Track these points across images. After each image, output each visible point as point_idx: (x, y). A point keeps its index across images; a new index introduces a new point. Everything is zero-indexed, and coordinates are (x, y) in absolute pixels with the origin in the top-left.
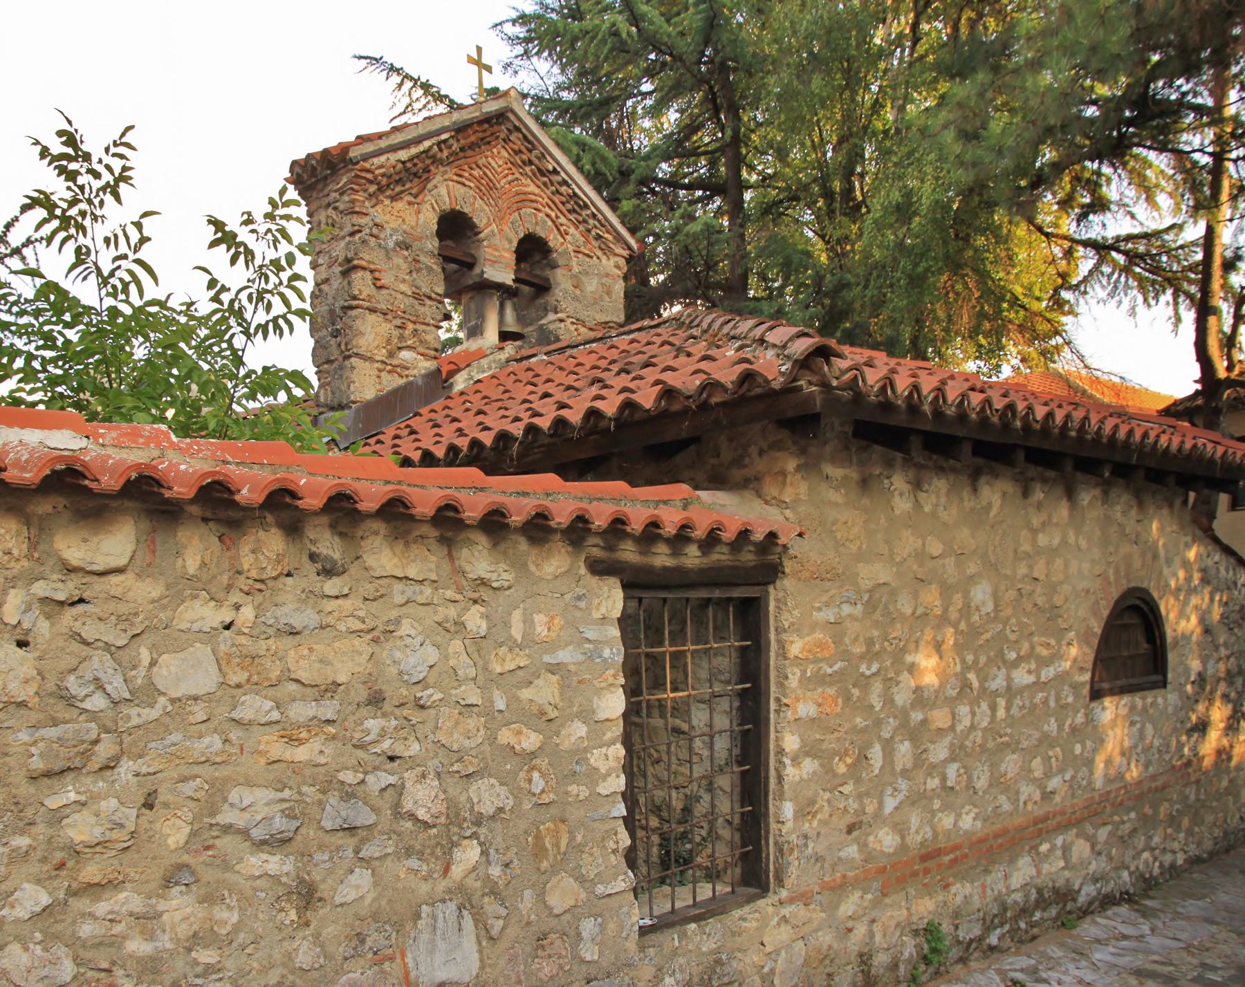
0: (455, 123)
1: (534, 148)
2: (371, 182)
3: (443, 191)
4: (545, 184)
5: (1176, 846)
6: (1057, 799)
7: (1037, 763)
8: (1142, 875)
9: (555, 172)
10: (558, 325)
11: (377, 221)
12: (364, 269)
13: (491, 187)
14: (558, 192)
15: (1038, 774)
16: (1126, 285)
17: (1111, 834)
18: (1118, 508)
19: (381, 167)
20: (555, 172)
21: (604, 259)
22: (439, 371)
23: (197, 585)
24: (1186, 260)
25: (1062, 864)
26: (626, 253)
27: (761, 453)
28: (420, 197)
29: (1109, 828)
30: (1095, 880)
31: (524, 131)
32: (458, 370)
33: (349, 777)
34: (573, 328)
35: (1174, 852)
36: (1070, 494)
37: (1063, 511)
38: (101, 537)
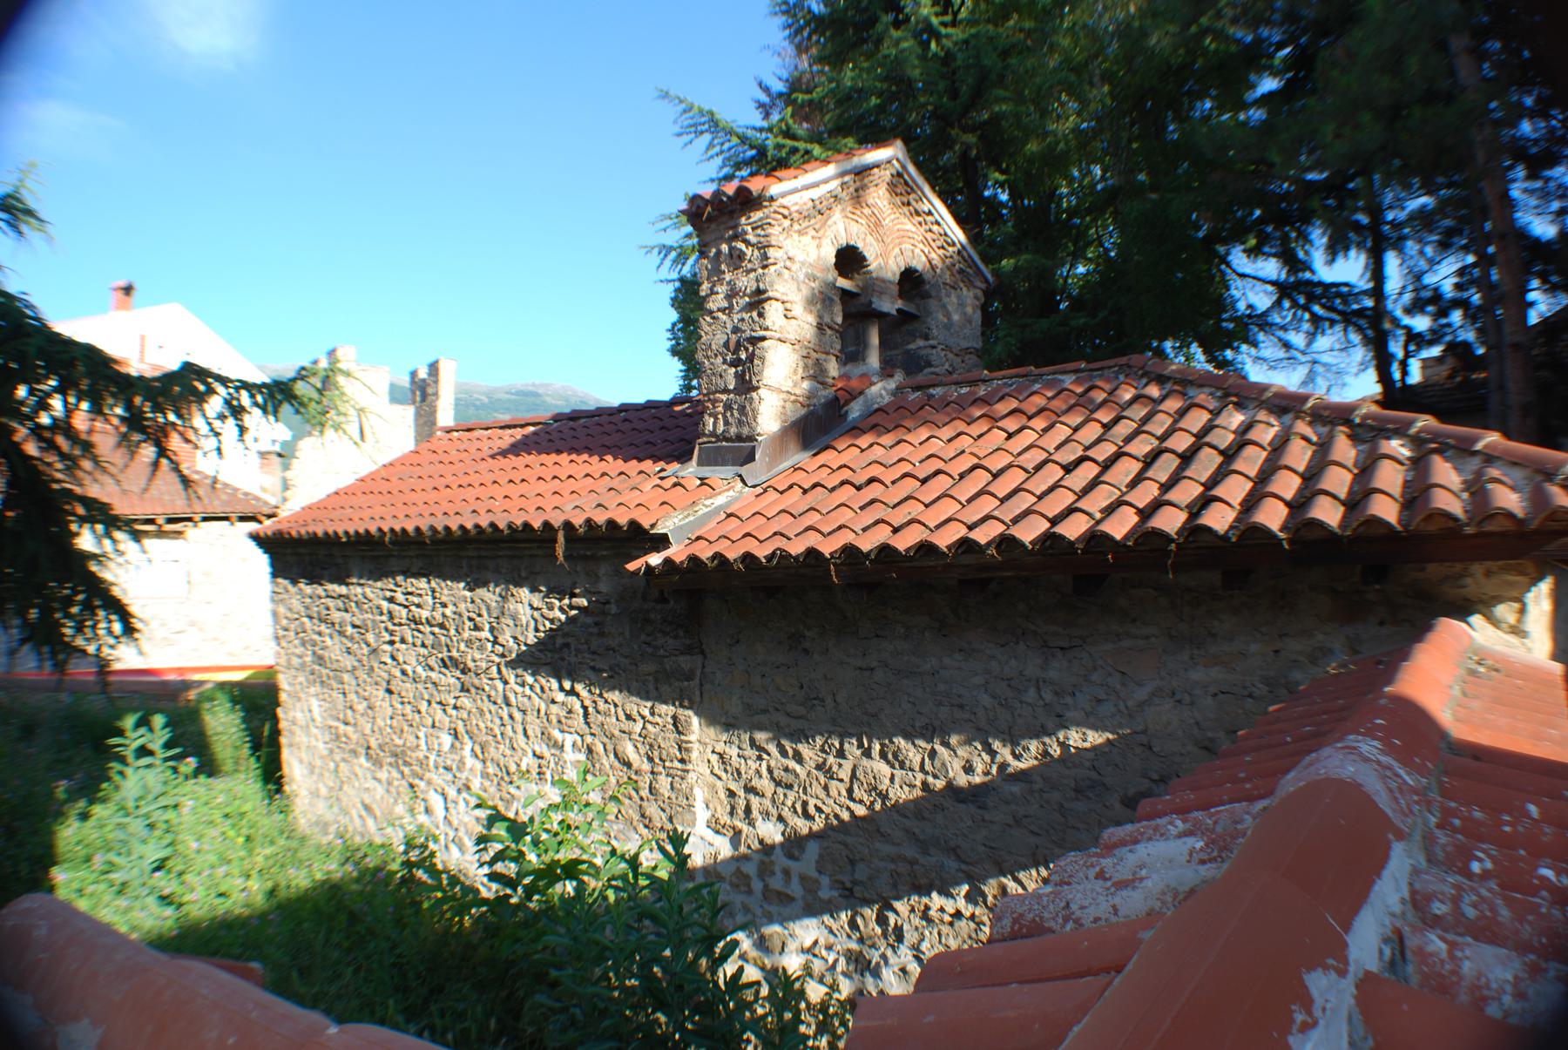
0: (855, 167)
2: (785, 217)
3: (841, 227)
4: (920, 224)
9: (930, 213)
10: (929, 351)
11: (790, 254)
12: (777, 300)
14: (930, 231)
19: (796, 204)
20: (930, 213)
21: (965, 289)
22: (836, 399)
24: (1274, 11)
26: (983, 286)
27: (1488, 574)
28: (821, 232)
31: (906, 177)
32: (854, 398)
34: (943, 354)
38: (210, 733)
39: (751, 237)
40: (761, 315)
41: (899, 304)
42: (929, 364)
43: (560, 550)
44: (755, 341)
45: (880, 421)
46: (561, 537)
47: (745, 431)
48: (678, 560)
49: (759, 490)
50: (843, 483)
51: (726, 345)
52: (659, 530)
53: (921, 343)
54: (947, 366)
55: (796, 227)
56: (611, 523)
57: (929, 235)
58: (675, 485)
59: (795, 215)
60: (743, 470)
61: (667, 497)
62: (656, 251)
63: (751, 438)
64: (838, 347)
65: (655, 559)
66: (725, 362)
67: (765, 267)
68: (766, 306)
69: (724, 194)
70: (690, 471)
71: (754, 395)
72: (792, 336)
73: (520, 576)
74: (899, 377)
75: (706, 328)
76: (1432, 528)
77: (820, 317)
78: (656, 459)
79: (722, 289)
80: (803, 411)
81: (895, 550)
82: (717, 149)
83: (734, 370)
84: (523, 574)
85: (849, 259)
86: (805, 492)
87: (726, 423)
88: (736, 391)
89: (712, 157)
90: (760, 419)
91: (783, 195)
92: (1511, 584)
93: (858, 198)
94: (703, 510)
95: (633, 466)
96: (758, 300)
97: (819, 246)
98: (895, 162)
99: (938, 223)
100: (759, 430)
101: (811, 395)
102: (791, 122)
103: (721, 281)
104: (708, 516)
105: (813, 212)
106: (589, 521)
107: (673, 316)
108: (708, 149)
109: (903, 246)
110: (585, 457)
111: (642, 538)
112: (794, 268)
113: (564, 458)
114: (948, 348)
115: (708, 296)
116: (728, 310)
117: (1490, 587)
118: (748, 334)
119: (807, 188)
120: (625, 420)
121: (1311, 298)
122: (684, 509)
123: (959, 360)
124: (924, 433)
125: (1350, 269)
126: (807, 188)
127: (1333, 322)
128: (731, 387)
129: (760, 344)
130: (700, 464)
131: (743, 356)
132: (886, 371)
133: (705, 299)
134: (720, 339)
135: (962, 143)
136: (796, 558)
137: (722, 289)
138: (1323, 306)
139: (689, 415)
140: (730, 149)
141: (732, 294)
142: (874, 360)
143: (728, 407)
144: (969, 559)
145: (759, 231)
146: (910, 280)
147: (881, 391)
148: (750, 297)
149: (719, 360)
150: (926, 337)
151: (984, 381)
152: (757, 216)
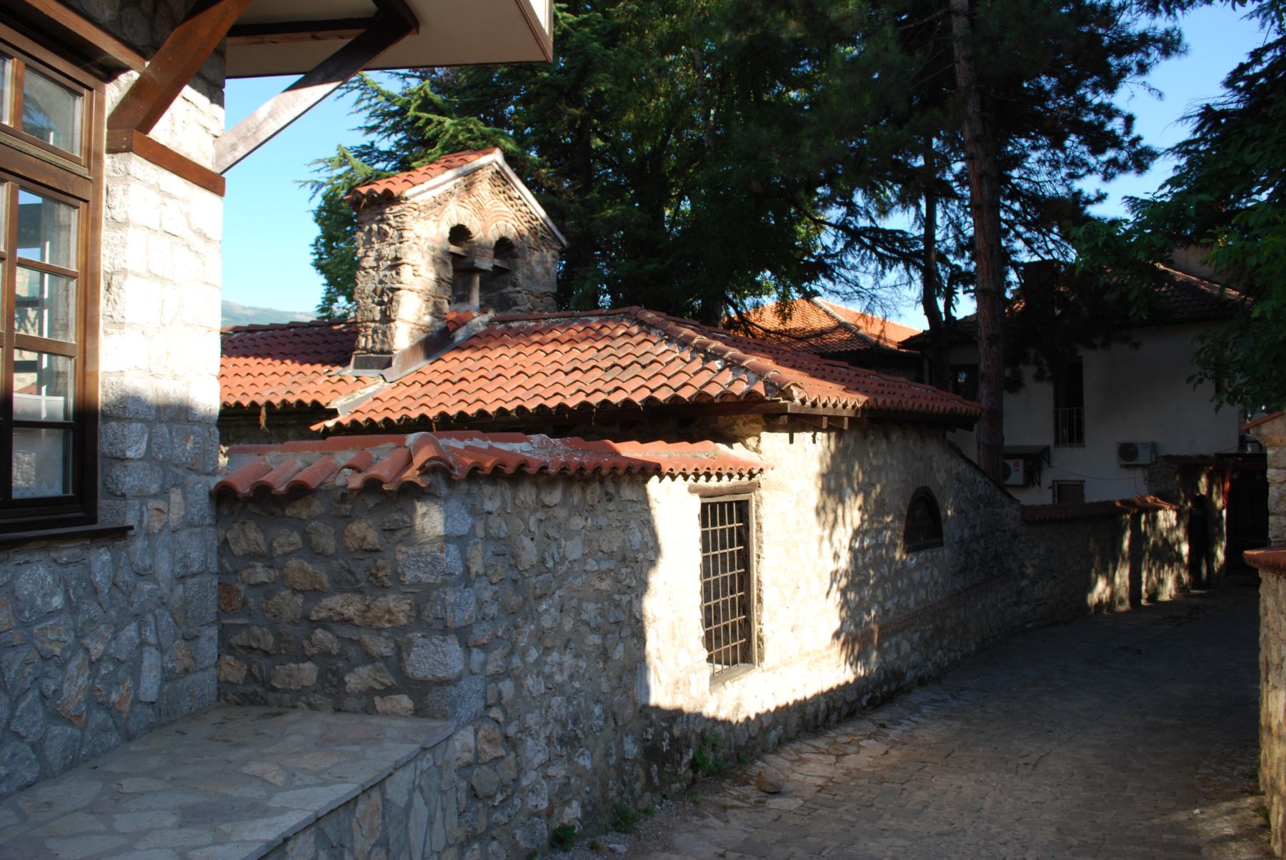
1: (507, 183)
5: (956, 648)
6: (891, 614)
7: (879, 592)
8: (939, 665)
9: (520, 198)
10: (516, 295)
13: (481, 208)
15: (880, 599)
16: (870, 258)
17: (921, 637)
18: (911, 442)
21: (545, 250)
22: (447, 328)
23: (576, 511)
25: (896, 656)
26: (559, 248)
27: (744, 424)
29: (919, 634)
30: (914, 668)
32: (459, 327)
33: (616, 597)
34: (526, 297)
35: (955, 651)
36: (887, 436)
37: (884, 446)
39: (392, 222)
40: (398, 274)
41: (497, 262)
42: (516, 304)
43: (263, 420)
44: (393, 290)
45: (476, 342)
46: (263, 412)
47: (386, 347)
48: (344, 423)
49: (395, 385)
50: (445, 381)
51: (375, 291)
52: (332, 406)
53: (510, 289)
54: (529, 305)
55: (423, 215)
56: (300, 403)
57: (519, 214)
58: (340, 380)
59: (422, 208)
60: (384, 372)
61: (335, 387)
62: (309, 185)
63: (390, 352)
64: (449, 294)
65: (330, 424)
66: (373, 302)
67: (401, 243)
68: (401, 268)
69: (375, 192)
70: (349, 372)
71: (392, 324)
72: (418, 288)
73: (228, 439)
74: (491, 314)
75: (362, 279)
76: (704, 401)
77: (438, 274)
78: (324, 364)
79: (372, 254)
80: (424, 336)
81: (466, 414)
82: (365, 103)
83: (379, 308)
84: (231, 438)
85: (459, 233)
86: (423, 385)
87: (374, 342)
88: (381, 321)
89: (360, 110)
90: (396, 340)
91: (414, 196)
92: (754, 429)
93: (469, 187)
94: (358, 396)
95: (307, 368)
96: (396, 264)
97: (438, 226)
98: (494, 164)
99: (525, 205)
100: (395, 347)
101: (432, 325)
102: (428, 90)
103: (372, 248)
104: (362, 399)
105: (434, 204)
106: (284, 401)
107: (316, 231)
108: (357, 103)
109: (499, 223)
110: (269, 360)
111: (320, 411)
112: (421, 242)
113: (251, 360)
114: (530, 293)
115: (362, 257)
116: (377, 268)
117: (745, 430)
118: (389, 285)
119: (429, 189)
120: (295, 335)
121: (875, 241)
122: (347, 395)
123: (539, 301)
124: (500, 351)
125: (902, 221)
126: (429, 189)
127: (896, 261)
128: (377, 319)
129: (397, 293)
130: (356, 367)
131: (386, 299)
132: (483, 309)
133: (361, 259)
134: (370, 287)
135: (570, 115)
136: (414, 420)
137: (372, 254)
138: (885, 248)
139: (345, 334)
140: (377, 104)
141: (379, 258)
142: (476, 300)
143: (375, 331)
144: (504, 419)
145: (398, 219)
146: (504, 246)
147: (479, 321)
148: (391, 261)
149: (370, 300)
150: (514, 285)
151: (544, 319)
152: (396, 208)
